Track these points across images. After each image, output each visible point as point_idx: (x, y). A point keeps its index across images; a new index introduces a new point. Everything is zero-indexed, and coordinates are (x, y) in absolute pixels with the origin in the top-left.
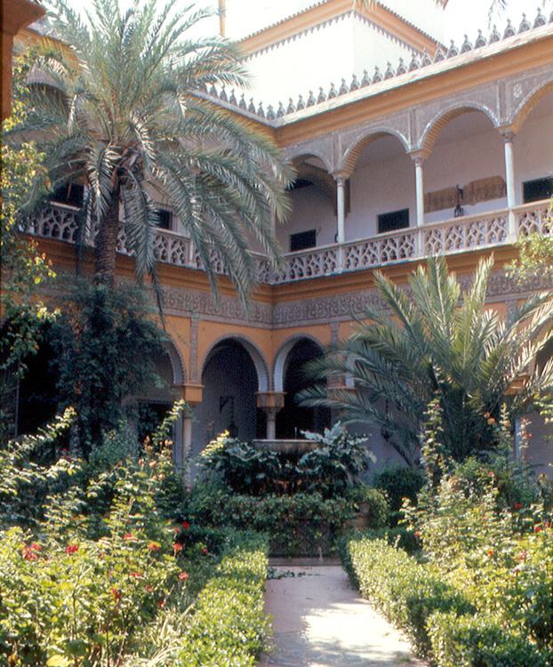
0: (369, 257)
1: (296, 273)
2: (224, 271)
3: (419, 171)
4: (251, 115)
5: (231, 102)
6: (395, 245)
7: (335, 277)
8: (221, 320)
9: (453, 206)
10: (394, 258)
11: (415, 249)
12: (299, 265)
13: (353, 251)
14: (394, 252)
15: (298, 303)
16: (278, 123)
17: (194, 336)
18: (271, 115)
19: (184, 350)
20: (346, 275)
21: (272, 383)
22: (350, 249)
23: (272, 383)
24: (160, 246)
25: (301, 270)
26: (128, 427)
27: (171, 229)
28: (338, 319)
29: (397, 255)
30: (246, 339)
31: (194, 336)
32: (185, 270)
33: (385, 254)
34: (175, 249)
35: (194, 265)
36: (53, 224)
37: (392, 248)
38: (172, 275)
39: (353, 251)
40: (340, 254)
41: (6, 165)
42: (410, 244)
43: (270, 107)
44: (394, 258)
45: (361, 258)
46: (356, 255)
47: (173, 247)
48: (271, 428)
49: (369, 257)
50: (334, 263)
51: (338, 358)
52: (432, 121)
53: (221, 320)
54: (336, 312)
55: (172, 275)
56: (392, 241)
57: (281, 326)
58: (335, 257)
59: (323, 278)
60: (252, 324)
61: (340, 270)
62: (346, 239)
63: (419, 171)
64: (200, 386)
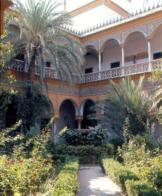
0: (108, 76)
1: (87, 80)
2: (66, 80)
3: (123, 50)
4: (73, 34)
5: (68, 30)
6: (116, 72)
7: (98, 81)
8: (65, 94)
9: (133, 61)
10: (116, 76)
11: (122, 73)
12: (88, 78)
13: (103, 74)
14: (115, 74)
15: (87, 89)
16: (81, 36)
17: (57, 99)
18: (79, 34)
19: (54, 103)
20: (101, 81)
21: (80, 113)
22: (103, 73)
23: (80, 113)
24: (47, 72)
25: (88, 79)
26: (37, 125)
27: (50, 67)
28: (99, 94)
29: (116, 75)
30: (72, 100)
31: (57, 99)
32: (54, 79)
33: (113, 75)
34: (51, 73)
35: (57, 78)
36: (16, 66)
37: (115, 73)
38: (50, 81)
39: (103, 74)
40: (100, 75)
41: (2, 49)
42: (120, 72)
43: (79, 32)
44: (116, 76)
45: (106, 76)
46: (104, 75)
47: (51, 72)
48: (80, 126)
49: (108, 76)
50: (98, 77)
51: (99, 105)
52: (126, 36)
53: (65, 94)
54: (98, 92)
55: (50, 81)
56: (115, 71)
57: (82, 96)
58: (98, 75)
59: (95, 82)
60: (74, 95)
61: (99, 79)
62: (101, 70)
63: (123, 50)
64: (59, 113)
